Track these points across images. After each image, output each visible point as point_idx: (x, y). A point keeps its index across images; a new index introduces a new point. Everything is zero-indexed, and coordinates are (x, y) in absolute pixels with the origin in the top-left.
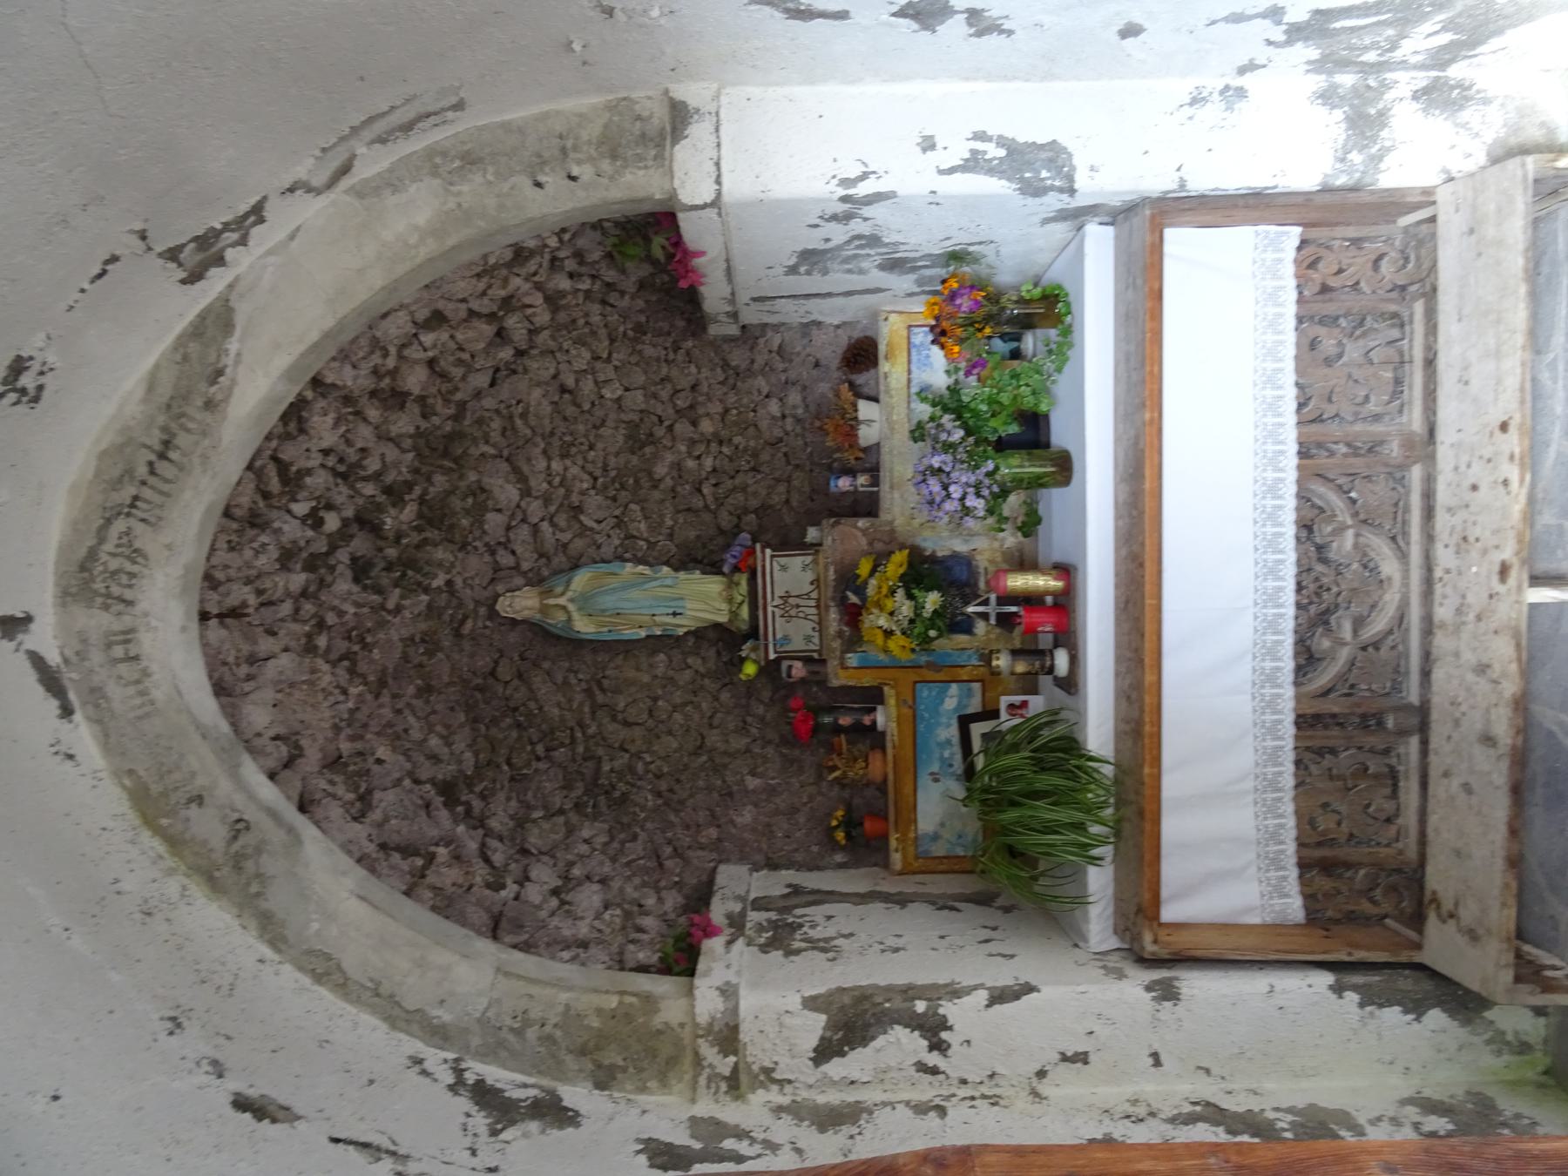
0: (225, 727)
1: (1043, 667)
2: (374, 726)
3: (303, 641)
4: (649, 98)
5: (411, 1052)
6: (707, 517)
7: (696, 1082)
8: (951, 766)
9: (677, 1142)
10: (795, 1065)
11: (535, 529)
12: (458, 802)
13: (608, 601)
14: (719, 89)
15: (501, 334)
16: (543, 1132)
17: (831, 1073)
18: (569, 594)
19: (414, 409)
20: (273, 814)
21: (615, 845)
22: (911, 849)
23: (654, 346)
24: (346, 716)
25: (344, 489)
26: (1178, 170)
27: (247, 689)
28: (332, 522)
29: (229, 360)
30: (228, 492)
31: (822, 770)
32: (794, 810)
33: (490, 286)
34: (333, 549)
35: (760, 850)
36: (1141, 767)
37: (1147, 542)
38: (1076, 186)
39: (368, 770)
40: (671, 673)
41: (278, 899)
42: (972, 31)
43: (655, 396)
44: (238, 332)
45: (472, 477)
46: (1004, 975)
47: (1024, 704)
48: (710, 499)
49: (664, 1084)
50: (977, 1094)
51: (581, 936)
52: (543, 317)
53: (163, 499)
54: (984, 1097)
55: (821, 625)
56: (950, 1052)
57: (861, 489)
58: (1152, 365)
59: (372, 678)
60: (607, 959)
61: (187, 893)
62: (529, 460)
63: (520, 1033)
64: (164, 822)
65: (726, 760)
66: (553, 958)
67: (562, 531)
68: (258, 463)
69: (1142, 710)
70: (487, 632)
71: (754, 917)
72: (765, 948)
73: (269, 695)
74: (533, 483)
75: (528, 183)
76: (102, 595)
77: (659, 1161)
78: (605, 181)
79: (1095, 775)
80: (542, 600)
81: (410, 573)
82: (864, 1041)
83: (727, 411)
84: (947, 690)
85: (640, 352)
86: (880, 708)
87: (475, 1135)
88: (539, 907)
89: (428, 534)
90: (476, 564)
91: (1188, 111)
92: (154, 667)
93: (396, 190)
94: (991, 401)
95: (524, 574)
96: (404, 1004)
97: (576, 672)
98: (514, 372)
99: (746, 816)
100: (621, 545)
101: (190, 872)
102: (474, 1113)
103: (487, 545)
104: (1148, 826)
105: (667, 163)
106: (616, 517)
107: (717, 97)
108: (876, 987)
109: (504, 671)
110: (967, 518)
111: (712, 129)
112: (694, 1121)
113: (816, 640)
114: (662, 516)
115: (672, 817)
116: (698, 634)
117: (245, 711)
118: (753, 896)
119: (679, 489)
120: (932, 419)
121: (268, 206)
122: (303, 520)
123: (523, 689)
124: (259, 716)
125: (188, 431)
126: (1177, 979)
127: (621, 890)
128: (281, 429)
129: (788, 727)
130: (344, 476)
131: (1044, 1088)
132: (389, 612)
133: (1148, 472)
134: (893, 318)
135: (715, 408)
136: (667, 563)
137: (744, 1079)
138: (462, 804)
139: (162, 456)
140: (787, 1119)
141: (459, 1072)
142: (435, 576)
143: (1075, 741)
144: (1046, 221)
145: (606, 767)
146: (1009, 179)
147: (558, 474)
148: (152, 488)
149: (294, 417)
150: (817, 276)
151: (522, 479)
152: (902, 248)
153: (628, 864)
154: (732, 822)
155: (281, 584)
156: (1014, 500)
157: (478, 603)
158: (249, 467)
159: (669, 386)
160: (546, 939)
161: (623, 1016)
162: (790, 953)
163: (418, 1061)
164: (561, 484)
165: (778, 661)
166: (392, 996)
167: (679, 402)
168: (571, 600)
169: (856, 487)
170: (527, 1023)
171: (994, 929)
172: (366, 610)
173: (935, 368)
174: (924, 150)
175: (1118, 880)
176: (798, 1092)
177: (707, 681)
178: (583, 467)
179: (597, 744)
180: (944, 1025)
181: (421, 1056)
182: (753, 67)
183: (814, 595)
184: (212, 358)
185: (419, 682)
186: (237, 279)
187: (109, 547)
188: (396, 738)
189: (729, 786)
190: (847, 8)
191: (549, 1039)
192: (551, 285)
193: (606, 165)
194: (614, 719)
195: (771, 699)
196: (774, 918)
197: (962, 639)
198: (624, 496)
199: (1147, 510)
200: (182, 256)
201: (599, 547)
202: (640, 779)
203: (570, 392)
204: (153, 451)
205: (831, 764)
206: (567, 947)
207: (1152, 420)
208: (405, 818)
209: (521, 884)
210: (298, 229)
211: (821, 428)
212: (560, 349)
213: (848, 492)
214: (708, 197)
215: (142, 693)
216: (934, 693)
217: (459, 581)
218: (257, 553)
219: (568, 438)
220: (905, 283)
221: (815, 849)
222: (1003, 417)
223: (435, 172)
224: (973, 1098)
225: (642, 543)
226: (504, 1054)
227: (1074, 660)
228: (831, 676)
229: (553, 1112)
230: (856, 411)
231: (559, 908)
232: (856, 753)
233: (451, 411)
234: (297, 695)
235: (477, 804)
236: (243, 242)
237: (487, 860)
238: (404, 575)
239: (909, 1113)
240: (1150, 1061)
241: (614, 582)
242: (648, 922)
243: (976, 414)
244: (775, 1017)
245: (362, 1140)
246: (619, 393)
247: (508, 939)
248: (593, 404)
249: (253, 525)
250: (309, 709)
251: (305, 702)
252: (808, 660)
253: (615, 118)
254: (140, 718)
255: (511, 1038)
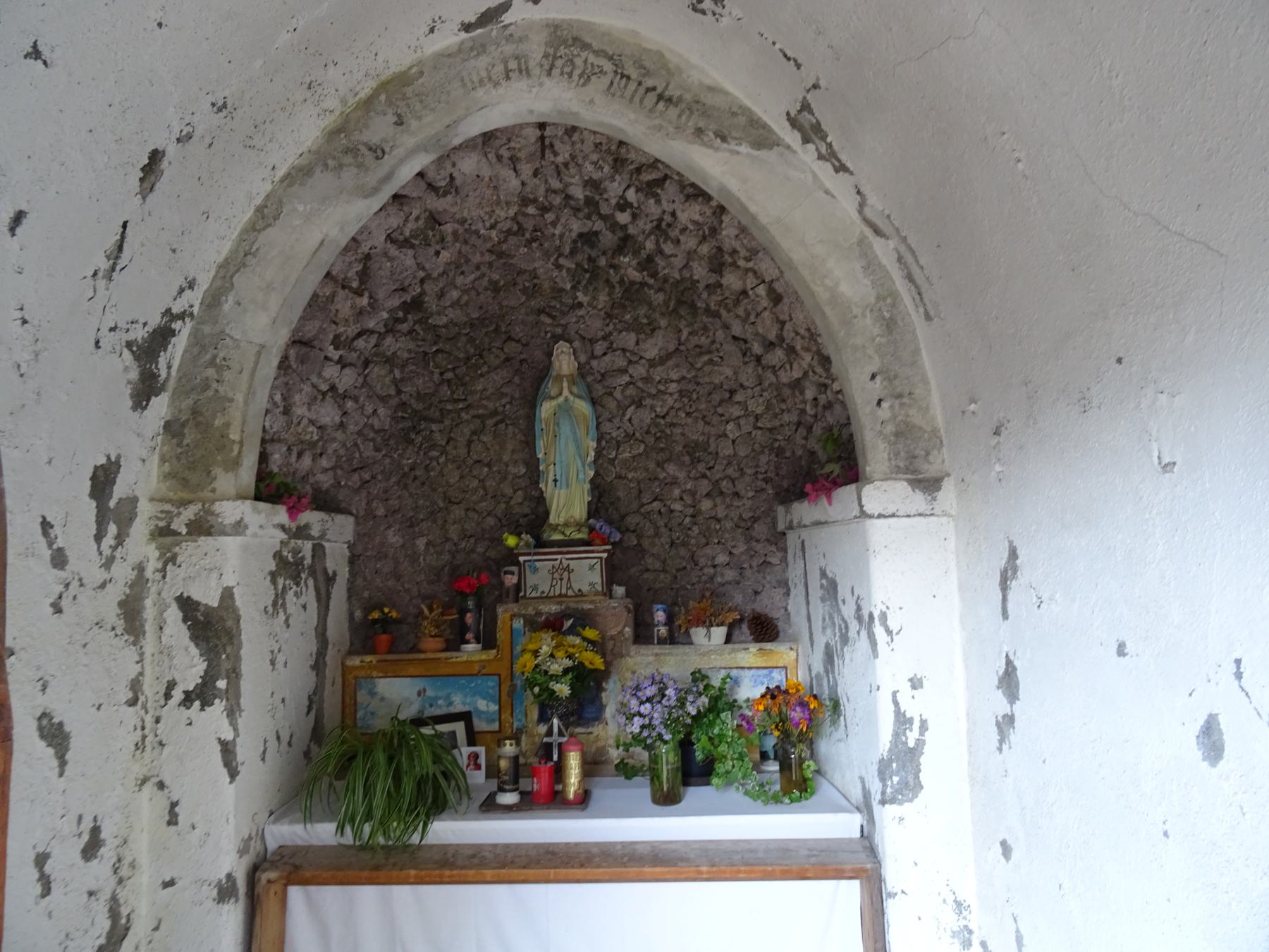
0: (457, 141)
1: (504, 782)
2: (465, 249)
3: (531, 196)
4: (943, 461)
5: (199, 280)
6: (635, 506)
7: (167, 502)
8: (431, 706)
9: (115, 488)
10: (177, 582)
11: (623, 371)
12: (406, 313)
13: (565, 429)
14: (952, 516)
15: (770, 345)
16: (129, 382)
17: (169, 611)
18: (571, 398)
19: (713, 279)
20: (388, 177)
21: (372, 435)
22: (362, 673)
23: (768, 463)
24: (473, 228)
25: (648, 227)
26: (903, 892)
27: (490, 156)
28: (623, 218)
29: (733, 146)
30: (635, 143)
31: (429, 599)
32: (398, 577)
33: (803, 338)
34: (604, 218)
35: (366, 549)
36: (416, 868)
37: (601, 870)
38: (887, 806)
39: (429, 245)
40: (510, 477)
41: (322, 181)
42: (1000, 719)
43: (729, 464)
44: (756, 153)
45: (663, 323)
46: (246, 752)
47: (478, 767)
48: (648, 508)
49: (166, 476)
50: (146, 731)
51: (294, 409)
52: (785, 377)
53: (628, 97)
54: (144, 737)
55: (546, 598)
56: (182, 708)
57: (656, 629)
58: (745, 872)
59: (504, 247)
60: (275, 430)
61: (327, 113)
62: (677, 366)
63: (212, 363)
64: (383, 97)
65: (440, 522)
66: (273, 387)
67: (623, 391)
68: (659, 165)
69: (463, 868)
70: (543, 334)
71: (307, 547)
72: (278, 556)
73: (486, 172)
74: (659, 369)
75: (874, 369)
76: (555, 53)
77: (100, 473)
78: (878, 427)
79: (411, 828)
80: (566, 376)
81: (587, 275)
82: (195, 638)
83: (719, 521)
84: (493, 702)
85: (763, 452)
86: (480, 646)
87: (128, 330)
88: (320, 375)
89: (617, 290)
90: (595, 325)
91: (950, 899)
92: (501, 91)
93: (865, 268)
94: (721, 736)
95: (588, 363)
96: (237, 275)
97: (510, 403)
98: (744, 355)
99: (394, 538)
100: (612, 438)
101: (344, 115)
102: (146, 329)
103: (611, 333)
104: (366, 874)
105: (894, 475)
106: (634, 434)
107: (945, 514)
108: (240, 648)
109: (511, 348)
110: (624, 718)
111: (921, 511)
112: (134, 501)
113: (533, 595)
114: (635, 470)
115: (394, 479)
116: (541, 500)
117: (472, 155)
118: (326, 545)
119: (657, 483)
120: (707, 687)
121: (846, 175)
122: (623, 197)
123: (497, 362)
124: (469, 165)
125: (680, 116)
126: (237, 901)
127: (334, 440)
128: (687, 183)
129: (465, 572)
130: (658, 227)
131: (149, 788)
132: (557, 260)
133: (658, 869)
134: (793, 654)
135: (721, 512)
136: (597, 474)
137: (169, 540)
138: (405, 315)
139: (660, 97)
140: (132, 575)
141: (181, 316)
142: (585, 294)
143: (443, 811)
144: (862, 780)
145: (434, 427)
146: (890, 750)
147: (667, 388)
148: (636, 91)
149: (696, 193)
150: (820, 593)
151: (663, 360)
152: (841, 662)
153: (356, 445)
154: (389, 527)
155: (573, 181)
156: (642, 755)
157: (565, 326)
158: (657, 161)
159: (737, 475)
160: (291, 382)
161: (223, 442)
162: (273, 576)
163: (191, 285)
164: (660, 391)
165: (518, 563)
166: (244, 265)
167: (725, 482)
168: (566, 400)
169: (657, 625)
170: (220, 369)
171: (290, 744)
172: (558, 242)
173: (750, 690)
174: (911, 680)
175: (324, 848)
176: (156, 583)
177: (503, 506)
178: (672, 408)
179: (453, 420)
180: (206, 703)
181: (196, 288)
182: (968, 544)
183: (570, 593)
184: (734, 134)
185: (502, 283)
186: (794, 152)
187: (592, 58)
188: (458, 265)
189: (418, 525)
190: (1010, 618)
191: (206, 385)
192: (807, 384)
193: (890, 428)
194: (474, 433)
195: (489, 558)
196: (305, 562)
197: (534, 714)
198: (650, 440)
199: (628, 869)
200: (806, 113)
201: (610, 420)
202: (425, 454)
203: (730, 398)
204: (664, 91)
205: (435, 606)
206: (284, 399)
207: (700, 873)
208: (392, 273)
209: (338, 362)
210: (833, 196)
211: (703, 596)
212: (763, 390)
213: (653, 619)
214: (868, 508)
215: (481, 81)
216: (490, 691)
217: (581, 312)
218: (595, 163)
219: (695, 396)
220: (818, 667)
221: (366, 594)
222: (709, 746)
223: (879, 298)
224: (143, 728)
225: (614, 453)
226: (196, 350)
227: (509, 809)
228: (505, 607)
229: (145, 390)
230: (718, 625)
231: (319, 391)
232: (442, 628)
233: (713, 307)
234: (489, 192)
235: (404, 327)
236: (821, 157)
237: (359, 335)
238: (586, 271)
239: (133, 676)
240: (168, 879)
241: (581, 432)
242: (307, 461)
243: (711, 724)
244: (217, 565)
245: (125, 245)
246: (731, 436)
247: (292, 352)
248: (722, 415)
249: (616, 160)
250: (478, 201)
251: (483, 198)
252: (518, 587)
253: (926, 435)
254: (462, 80)
255: (208, 357)
